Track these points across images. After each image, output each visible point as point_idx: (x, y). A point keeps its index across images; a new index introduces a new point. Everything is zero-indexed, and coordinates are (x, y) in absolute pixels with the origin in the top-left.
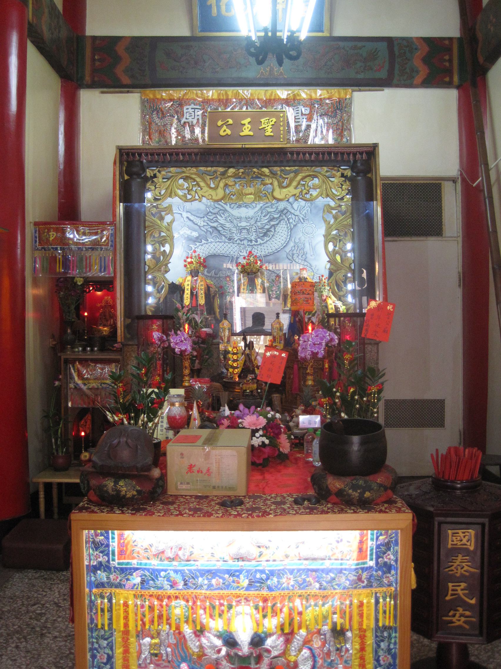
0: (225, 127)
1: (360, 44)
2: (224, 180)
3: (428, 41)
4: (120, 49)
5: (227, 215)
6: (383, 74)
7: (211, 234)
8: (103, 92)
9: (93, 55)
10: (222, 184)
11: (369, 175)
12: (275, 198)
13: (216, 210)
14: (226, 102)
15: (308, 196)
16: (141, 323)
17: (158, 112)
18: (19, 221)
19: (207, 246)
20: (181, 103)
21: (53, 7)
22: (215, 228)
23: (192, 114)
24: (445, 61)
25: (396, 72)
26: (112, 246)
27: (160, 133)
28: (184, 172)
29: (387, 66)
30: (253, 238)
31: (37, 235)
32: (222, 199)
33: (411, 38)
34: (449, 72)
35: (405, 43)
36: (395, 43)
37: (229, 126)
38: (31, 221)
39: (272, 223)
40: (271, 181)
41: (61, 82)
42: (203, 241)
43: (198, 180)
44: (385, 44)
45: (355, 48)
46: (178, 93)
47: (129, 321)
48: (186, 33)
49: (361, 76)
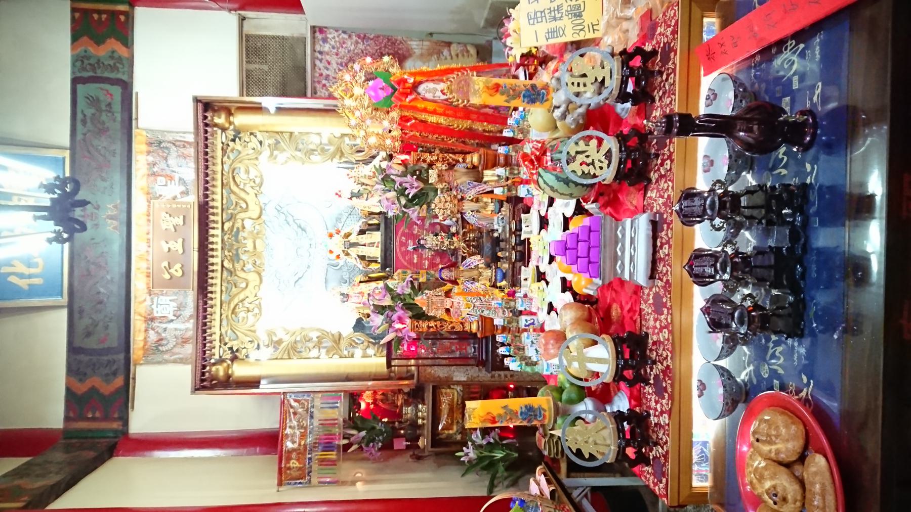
0: (172, 271)
1: (79, 116)
2: (238, 273)
3: (75, 38)
4: (81, 388)
6: (116, 91)
8: (133, 407)
9: (88, 419)
10: (242, 274)
12: (259, 217)
15: (258, 181)
17: (160, 345)
20: (150, 319)
21: (16, 473)
23: (165, 305)
24: (100, 18)
25: (112, 75)
26: (309, 396)
27: (185, 342)
28: (227, 316)
29: (107, 86)
31: (293, 482)
32: (259, 274)
33: (72, 56)
34: (115, 14)
35: (79, 64)
36: (79, 75)
38: (275, 490)
39: (291, 222)
40: (239, 221)
41: (117, 456)
43: (236, 301)
44: (80, 87)
45: (84, 122)
46: (137, 324)
48: (64, 313)
49: (118, 117)
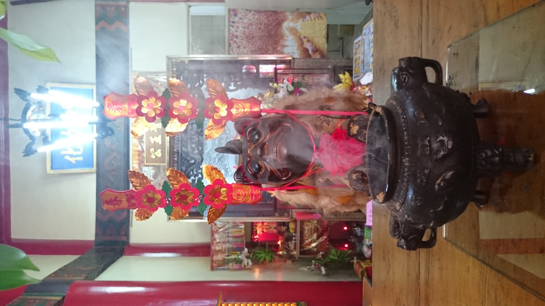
0: (156, 153)
5: (211, 153)
7: (222, 162)
8: (132, 226)
11: (187, 62)
13: (208, 159)
14: (140, 153)
16: (278, 207)
18: (214, 285)
19: (230, 165)
22: (219, 160)
30: (225, 136)
37: (155, 151)
42: (227, 167)
47: (277, 214)
